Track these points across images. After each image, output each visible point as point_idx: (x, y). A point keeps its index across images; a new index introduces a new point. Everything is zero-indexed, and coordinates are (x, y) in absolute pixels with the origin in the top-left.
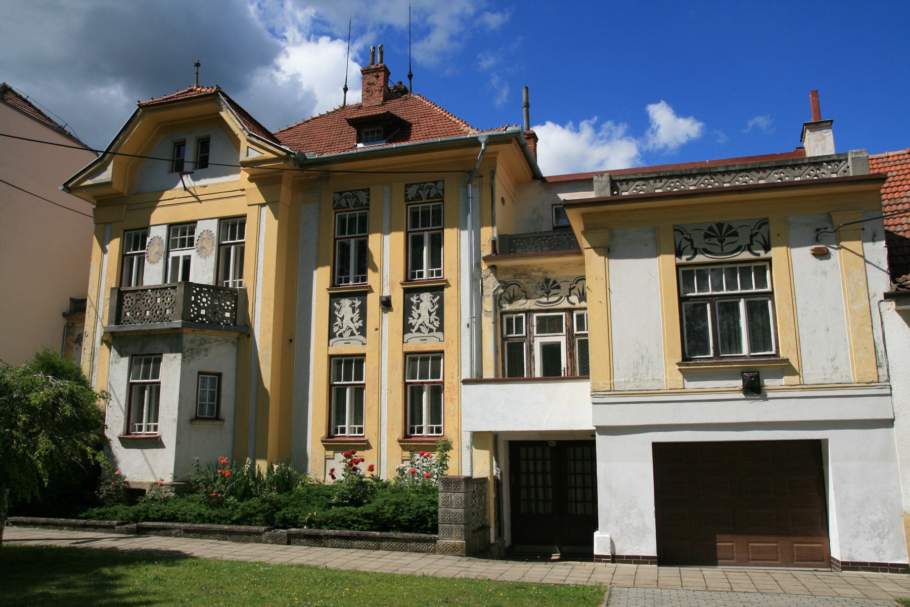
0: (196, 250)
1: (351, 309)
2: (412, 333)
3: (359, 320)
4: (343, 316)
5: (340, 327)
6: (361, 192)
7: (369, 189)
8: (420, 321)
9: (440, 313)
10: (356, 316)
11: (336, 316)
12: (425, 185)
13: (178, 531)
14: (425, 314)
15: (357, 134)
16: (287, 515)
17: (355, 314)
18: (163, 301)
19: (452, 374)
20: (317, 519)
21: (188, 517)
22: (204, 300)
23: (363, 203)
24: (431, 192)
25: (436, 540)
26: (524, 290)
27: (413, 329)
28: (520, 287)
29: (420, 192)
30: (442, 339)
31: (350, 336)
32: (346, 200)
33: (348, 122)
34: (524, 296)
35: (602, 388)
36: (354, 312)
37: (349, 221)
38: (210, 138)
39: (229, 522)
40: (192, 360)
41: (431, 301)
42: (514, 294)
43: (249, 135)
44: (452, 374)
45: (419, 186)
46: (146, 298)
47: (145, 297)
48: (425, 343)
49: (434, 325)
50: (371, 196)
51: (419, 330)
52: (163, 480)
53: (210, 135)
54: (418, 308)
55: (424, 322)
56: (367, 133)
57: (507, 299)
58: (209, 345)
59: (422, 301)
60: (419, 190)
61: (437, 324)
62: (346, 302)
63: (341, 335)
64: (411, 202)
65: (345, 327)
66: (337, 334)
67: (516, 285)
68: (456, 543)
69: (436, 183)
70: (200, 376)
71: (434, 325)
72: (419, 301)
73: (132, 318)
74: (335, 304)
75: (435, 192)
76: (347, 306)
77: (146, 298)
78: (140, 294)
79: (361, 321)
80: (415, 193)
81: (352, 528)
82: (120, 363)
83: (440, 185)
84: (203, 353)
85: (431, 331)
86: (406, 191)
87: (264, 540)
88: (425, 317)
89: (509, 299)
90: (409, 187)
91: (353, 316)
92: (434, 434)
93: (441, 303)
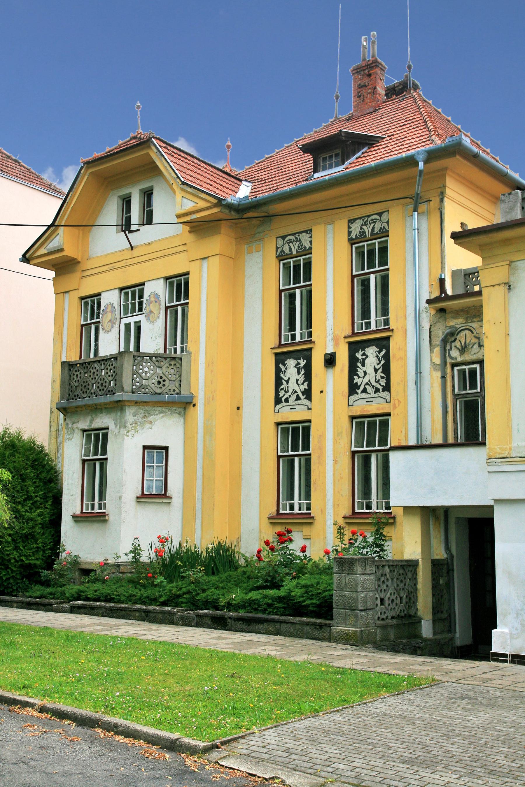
0: (144, 315)
1: (296, 369)
2: (357, 394)
3: (304, 382)
4: (289, 378)
5: (286, 392)
6: (304, 234)
7: (311, 230)
8: (366, 380)
9: (386, 369)
10: (301, 378)
11: (282, 378)
12: (370, 219)
13: (104, 610)
14: (369, 369)
15: (313, 163)
16: (209, 597)
17: (300, 375)
18: (107, 373)
19: (399, 440)
20: (235, 602)
21: (123, 598)
22: (146, 369)
23: (305, 247)
24: (376, 226)
25: (331, 627)
26: (477, 335)
27: (359, 389)
28: (472, 333)
29: (364, 227)
30: (388, 400)
31: (295, 401)
32: (289, 245)
33: (301, 150)
34: (477, 344)
35: (500, 454)
36: (299, 373)
37: (367, 255)
38: (153, 190)
39: (158, 604)
40: (136, 434)
41: (377, 356)
42: (465, 342)
43: (182, 184)
44: (399, 440)
45: (363, 220)
46: (76, 374)
47: (91, 369)
48: (370, 405)
49: (380, 384)
50: (313, 239)
51: (365, 391)
52: (107, 560)
53: (153, 186)
54: (363, 365)
55: (369, 381)
56: (324, 159)
57: (458, 349)
58: (154, 417)
59: (367, 357)
60: (362, 225)
61: (383, 382)
62: (291, 363)
63: (287, 400)
64: (356, 241)
65: (290, 391)
66: (283, 399)
67: (467, 331)
68: (349, 630)
69: (380, 214)
70: (146, 451)
71: (380, 384)
72: (364, 357)
73: (98, 390)
74: (281, 365)
75: (380, 226)
76: (292, 366)
77: (92, 371)
78: (87, 367)
79: (306, 383)
80: (358, 229)
81: (267, 612)
82: (73, 440)
83: (384, 217)
84: (148, 426)
85: (377, 390)
86: (349, 228)
87: (175, 621)
88: (371, 376)
89: (460, 348)
90: (352, 223)
91: (298, 377)
92: (288, 511)
93: (387, 356)
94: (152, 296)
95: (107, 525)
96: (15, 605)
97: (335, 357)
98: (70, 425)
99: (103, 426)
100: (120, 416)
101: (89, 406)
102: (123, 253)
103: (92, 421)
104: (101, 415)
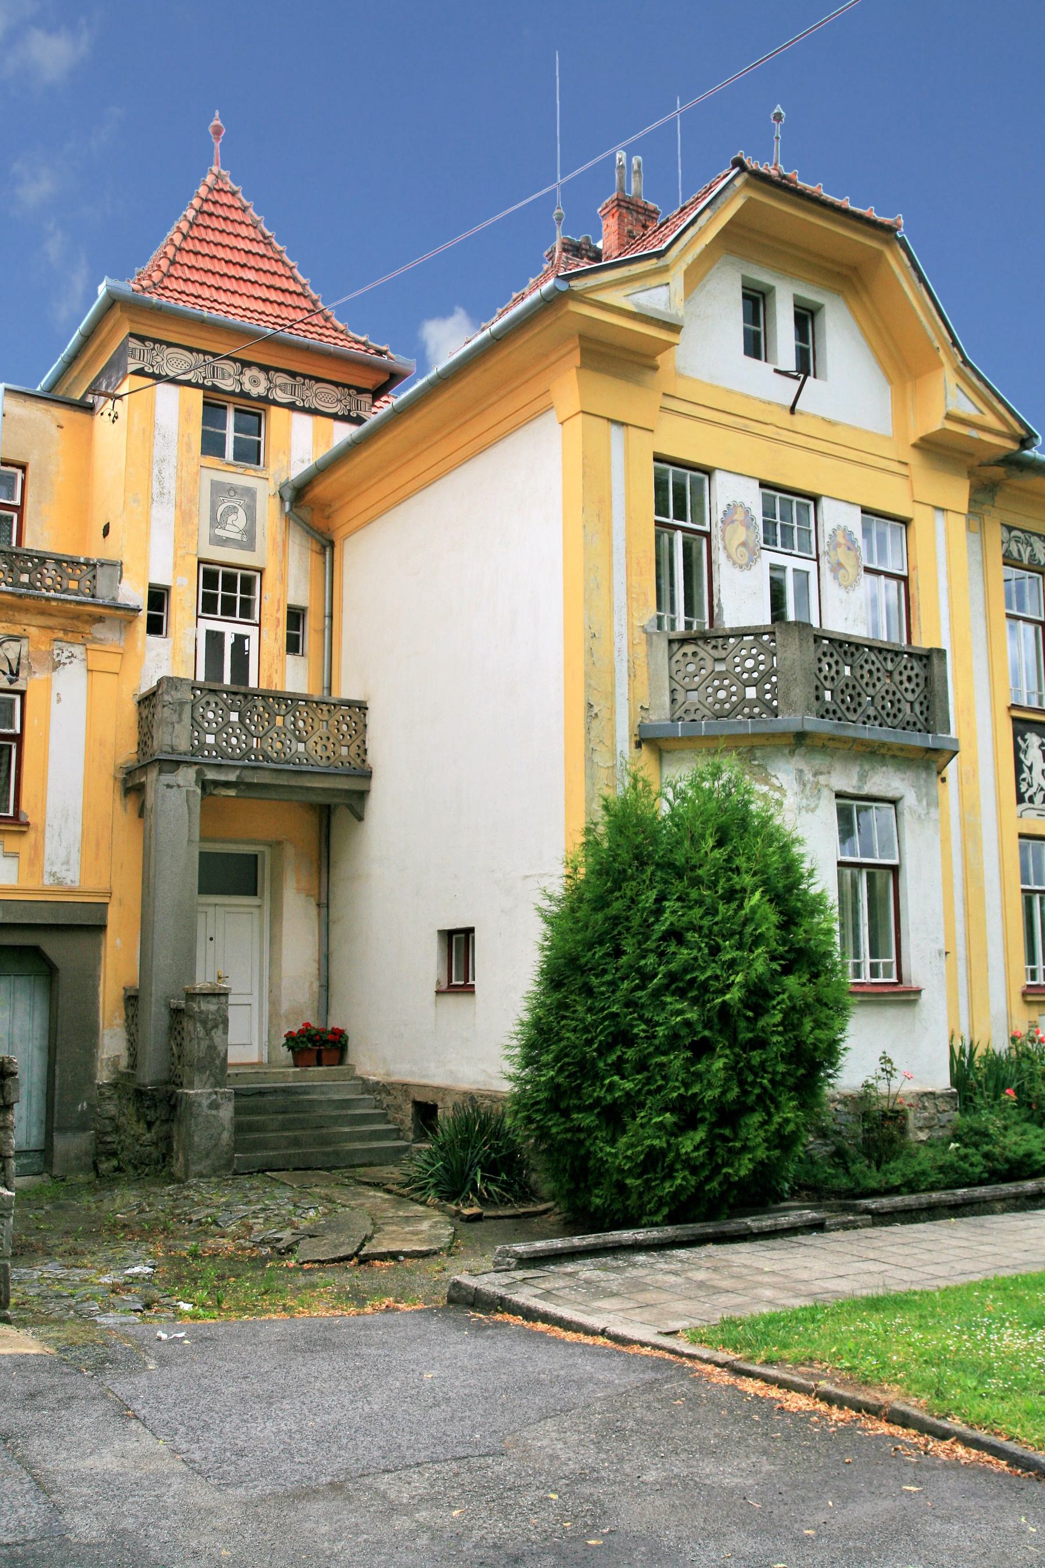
63: (1031, 800)
65: (1035, 786)
66: (1027, 796)
94: (839, 533)
95: (917, 1009)
96: (999, 1206)
97: (213, 632)
98: (808, 776)
99: (890, 794)
100: (926, 781)
101: (863, 742)
102: (769, 408)
103: (863, 778)
104: (884, 769)
